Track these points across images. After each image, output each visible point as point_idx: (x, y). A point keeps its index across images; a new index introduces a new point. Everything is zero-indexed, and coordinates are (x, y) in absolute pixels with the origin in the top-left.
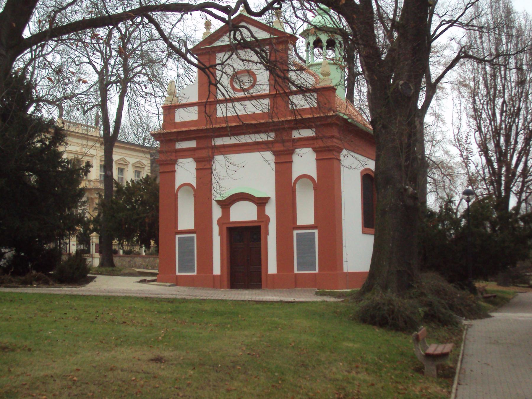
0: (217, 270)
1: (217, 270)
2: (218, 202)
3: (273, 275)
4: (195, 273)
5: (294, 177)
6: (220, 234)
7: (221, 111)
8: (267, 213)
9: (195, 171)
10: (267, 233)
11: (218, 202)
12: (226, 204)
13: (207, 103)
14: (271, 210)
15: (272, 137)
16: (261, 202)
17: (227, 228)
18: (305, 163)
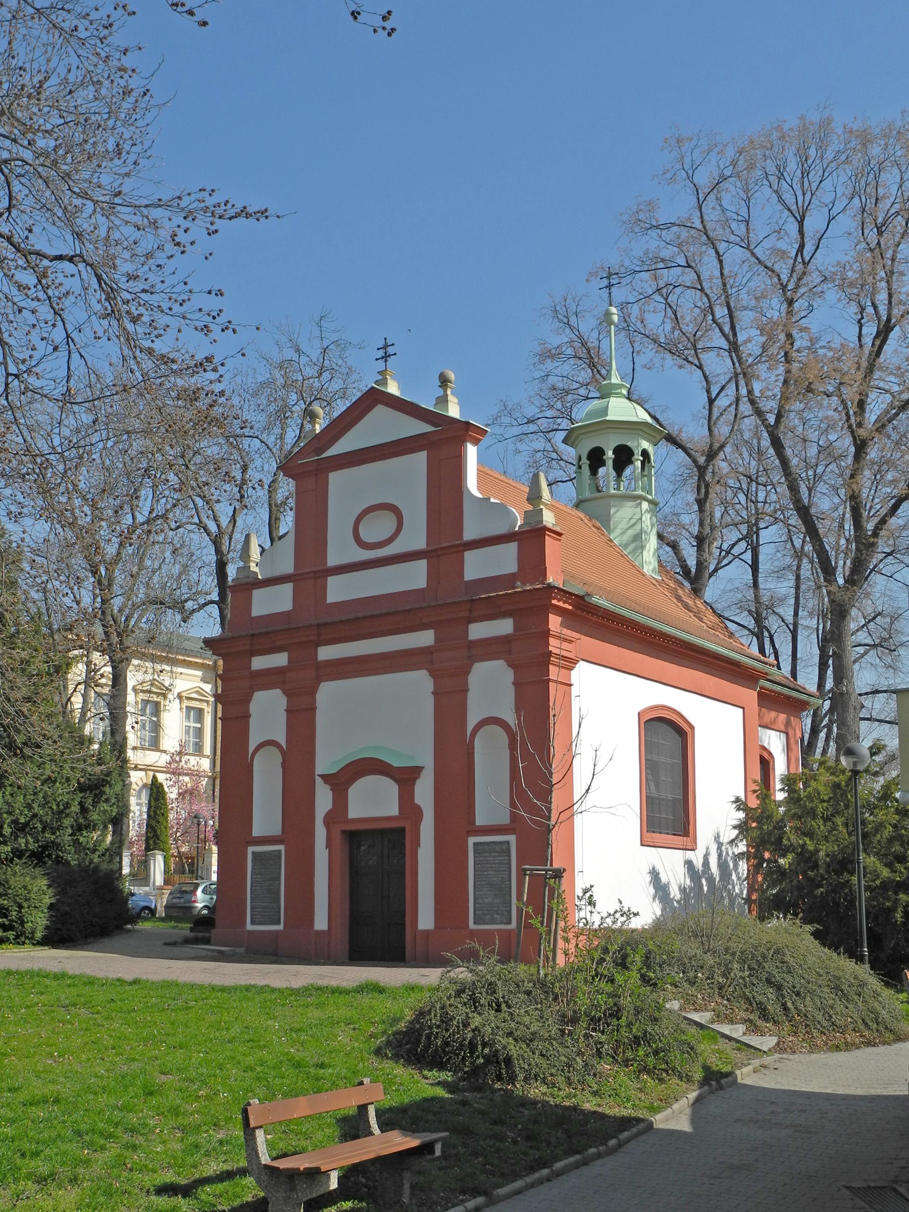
0: (321, 923)
1: (321, 923)
2: (321, 776)
3: (427, 933)
4: (281, 927)
5: (471, 725)
6: (329, 845)
7: (338, 590)
8: (418, 800)
9: (470, 686)
10: (417, 844)
11: (326, 778)
12: (340, 782)
13: (310, 573)
14: (424, 793)
15: (425, 638)
16: (405, 778)
17: (344, 832)
18: (491, 688)
